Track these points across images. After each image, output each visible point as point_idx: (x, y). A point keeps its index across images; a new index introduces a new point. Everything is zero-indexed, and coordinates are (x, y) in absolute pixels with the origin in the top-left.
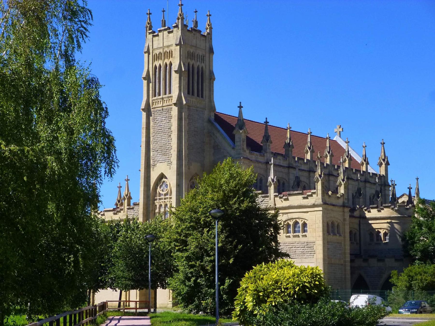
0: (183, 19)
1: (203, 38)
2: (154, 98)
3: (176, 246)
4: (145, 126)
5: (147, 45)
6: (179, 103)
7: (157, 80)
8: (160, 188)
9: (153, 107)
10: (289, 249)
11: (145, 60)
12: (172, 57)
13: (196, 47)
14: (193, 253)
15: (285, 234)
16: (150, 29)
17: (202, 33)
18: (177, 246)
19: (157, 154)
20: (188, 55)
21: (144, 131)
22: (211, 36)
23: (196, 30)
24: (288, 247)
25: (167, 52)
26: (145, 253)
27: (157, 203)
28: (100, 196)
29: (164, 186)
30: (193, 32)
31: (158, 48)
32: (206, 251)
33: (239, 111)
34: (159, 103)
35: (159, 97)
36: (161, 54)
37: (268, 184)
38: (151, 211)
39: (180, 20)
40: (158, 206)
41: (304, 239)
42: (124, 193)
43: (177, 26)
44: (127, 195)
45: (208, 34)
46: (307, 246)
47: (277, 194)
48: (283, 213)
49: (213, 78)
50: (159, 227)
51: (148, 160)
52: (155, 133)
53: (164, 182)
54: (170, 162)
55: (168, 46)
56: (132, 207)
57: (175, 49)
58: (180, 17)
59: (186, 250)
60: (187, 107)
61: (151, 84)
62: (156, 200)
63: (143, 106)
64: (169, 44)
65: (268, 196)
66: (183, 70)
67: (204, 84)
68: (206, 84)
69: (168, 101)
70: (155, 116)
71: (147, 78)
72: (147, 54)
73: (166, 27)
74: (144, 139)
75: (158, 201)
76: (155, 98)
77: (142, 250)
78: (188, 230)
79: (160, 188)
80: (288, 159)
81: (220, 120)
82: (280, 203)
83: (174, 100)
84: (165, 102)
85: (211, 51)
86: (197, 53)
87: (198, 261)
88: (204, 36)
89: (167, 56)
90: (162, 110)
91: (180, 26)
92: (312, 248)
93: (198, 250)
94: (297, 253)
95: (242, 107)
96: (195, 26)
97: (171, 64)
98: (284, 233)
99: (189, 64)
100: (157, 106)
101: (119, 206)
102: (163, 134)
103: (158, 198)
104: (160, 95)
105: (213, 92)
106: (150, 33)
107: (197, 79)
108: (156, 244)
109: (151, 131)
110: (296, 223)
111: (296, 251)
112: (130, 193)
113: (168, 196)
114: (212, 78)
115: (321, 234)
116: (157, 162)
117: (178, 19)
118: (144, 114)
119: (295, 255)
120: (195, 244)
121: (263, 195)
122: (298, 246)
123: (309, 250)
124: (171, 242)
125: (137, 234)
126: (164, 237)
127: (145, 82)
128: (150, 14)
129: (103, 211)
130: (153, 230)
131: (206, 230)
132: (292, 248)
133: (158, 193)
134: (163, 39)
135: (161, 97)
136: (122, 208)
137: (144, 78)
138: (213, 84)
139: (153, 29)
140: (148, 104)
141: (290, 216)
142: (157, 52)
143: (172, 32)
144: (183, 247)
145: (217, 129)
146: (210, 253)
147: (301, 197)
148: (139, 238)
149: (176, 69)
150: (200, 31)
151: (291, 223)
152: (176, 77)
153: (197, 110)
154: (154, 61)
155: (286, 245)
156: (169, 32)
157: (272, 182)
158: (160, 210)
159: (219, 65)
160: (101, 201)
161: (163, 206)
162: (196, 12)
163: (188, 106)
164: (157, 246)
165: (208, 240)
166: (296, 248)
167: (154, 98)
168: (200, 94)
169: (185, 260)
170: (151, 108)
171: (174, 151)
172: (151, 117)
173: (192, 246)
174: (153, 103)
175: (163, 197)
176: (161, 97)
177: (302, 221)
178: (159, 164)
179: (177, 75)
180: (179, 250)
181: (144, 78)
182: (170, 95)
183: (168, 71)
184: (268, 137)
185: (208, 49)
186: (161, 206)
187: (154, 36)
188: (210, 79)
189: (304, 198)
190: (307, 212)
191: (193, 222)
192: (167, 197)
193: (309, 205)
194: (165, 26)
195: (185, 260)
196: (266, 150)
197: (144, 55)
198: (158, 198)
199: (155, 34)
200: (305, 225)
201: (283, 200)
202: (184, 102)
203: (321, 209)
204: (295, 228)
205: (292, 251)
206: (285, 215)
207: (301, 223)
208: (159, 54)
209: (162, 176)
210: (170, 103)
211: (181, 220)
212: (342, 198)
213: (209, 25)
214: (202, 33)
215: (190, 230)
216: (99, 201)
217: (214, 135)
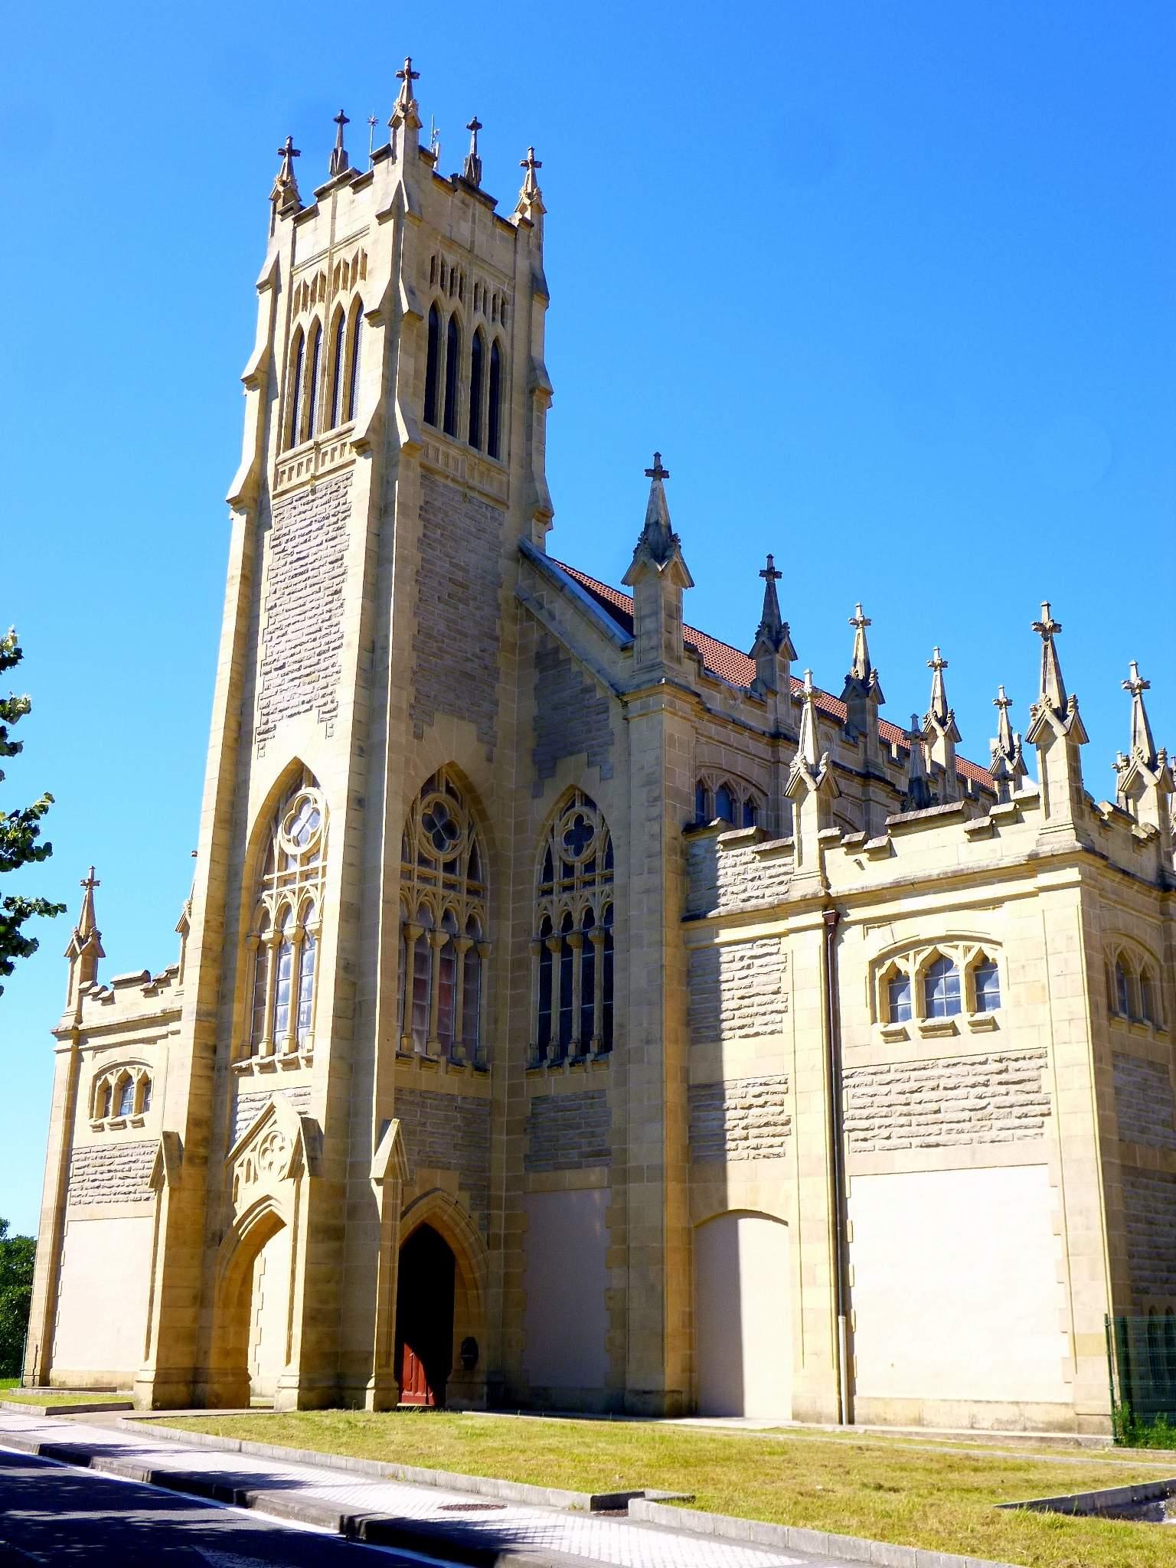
0: (414, 125)
1: (499, 230)
2: (283, 456)
4: (239, 572)
6: (377, 443)
7: (298, 389)
10: (902, 1099)
12: (364, 277)
15: (880, 1026)
17: (498, 210)
24: (899, 1087)
33: (653, 491)
37: (789, 787)
38: (241, 937)
40: (273, 915)
41: (986, 1043)
46: (1004, 1077)
47: (835, 831)
48: (868, 923)
51: (240, 725)
52: (278, 594)
53: (305, 800)
54: (330, 706)
55: (349, 241)
61: (276, 405)
62: (266, 886)
65: (791, 847)
67: (505, 408)
68: (512, 407)
71: (263, 380)
72: (268, 294)
75: (274, 891)
79: (288, 831)
80: (861, 745)
82: (848, 873)
84: (328, 458)
85: (538, 287)
89: (345, 281)
92: (1027, 1086)
94: (948, 1117)
98: (874, 1021)
99: (434, 309)
102: (309, 591)
103: (276, 874)
107: (469, 374)
109: (265, 588)
110: (937, 965)
111: (943, 1105)
114: (538, 389)
115: (1081, 1006)
117: (395, 124)
118: (239, 522)
119: (935, 1129)
121: (766, 846)
122: (951, 1083)
123: (1011, 1099)
132: (919, 1090)
134: (334, 217)
137: (250, 382)
138: (542, 422)
140: (257, 484)
141: (904, 931)
142: (307, 276)
147: (957, 832)
150: (490, 202)
151: (910, 966)
155: (888, 1077)
156: (357, 186)
157: (807, 778)
158: (280, 932)
161: (295, 911)
162: (476, 126)
166: (940, 1094)
168: (486, 436)
170: (271, 494)
172: (267, 534)
174: (278, 475)
177: (968, 949)
178: (286, 721)
184: (778, 633)
185: (522, 279)
186: (285, 910)
187: (298, 221)
189: (975, 834)
190: (996, 903)
193: (1006, 862)
196: (773, 682)
198: (276, 874)
200: (983, 970)
201: (863, 857)
203: (1073, 874)
204: (929, 993)
205: (919, 1108)
206: (874, 933)
207: (961, 959)
208: (315, 282)
209: (297, 777)
212: (1152, 846)
213: (529, 196)
214: (498, 210)
217: (541, 607)
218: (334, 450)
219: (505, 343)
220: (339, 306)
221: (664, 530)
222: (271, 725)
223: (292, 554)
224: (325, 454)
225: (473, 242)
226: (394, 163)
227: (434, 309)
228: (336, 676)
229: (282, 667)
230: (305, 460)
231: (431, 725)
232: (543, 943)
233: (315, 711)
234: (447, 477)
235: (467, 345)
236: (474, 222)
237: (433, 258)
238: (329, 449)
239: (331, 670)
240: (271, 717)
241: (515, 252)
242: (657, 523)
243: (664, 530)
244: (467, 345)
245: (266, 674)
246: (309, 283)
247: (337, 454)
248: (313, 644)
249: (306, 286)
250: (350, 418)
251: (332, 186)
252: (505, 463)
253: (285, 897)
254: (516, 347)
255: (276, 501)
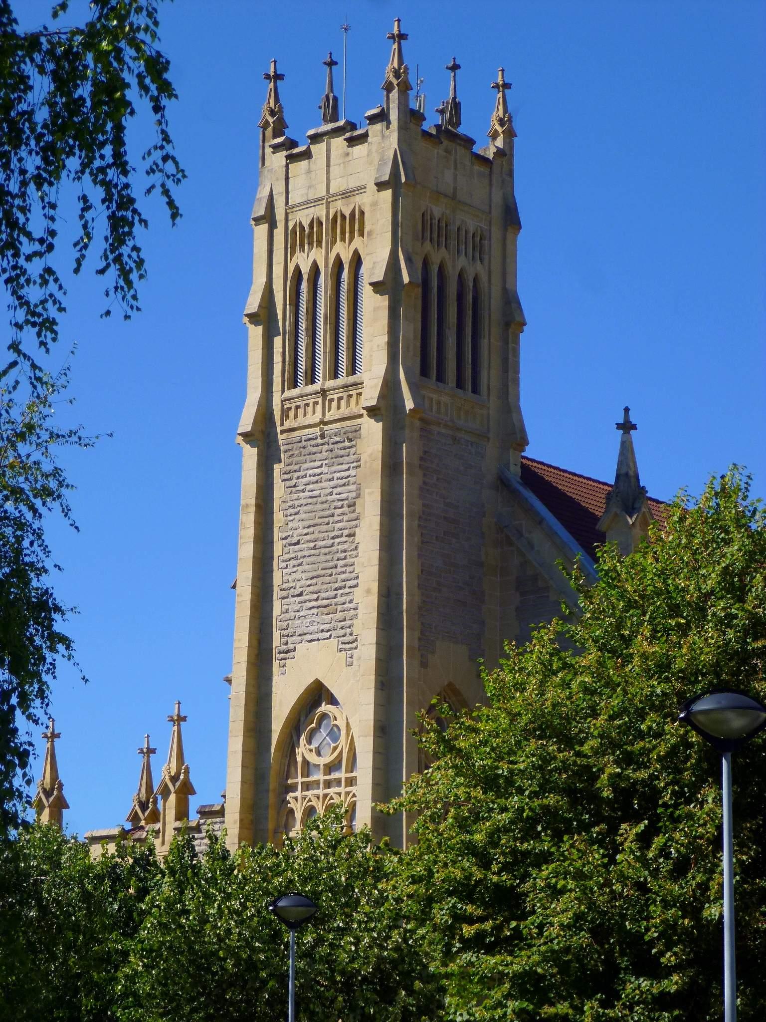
0: (405, 88)
1: (477, 168)
2: (288, 394)
3: (460, 918)
5: (264, 193)
6: (386, 408)
8: (309, 742)
9: (287, 425)
11: (256, 250)
12: (362, 234)
13: (454, 197)
14: (553, 957)
16: (276, 134)
17: (477, 149)
18: (471, 921)
19: (297, 607)
20: (424, 224)
21: (248, 521)
22: (511, 163)
23: (454, 137)
25: (343, 217)
26: (264, 982)
27: (296, 802)
28: (57, 609)
29: (323, 732)
30: (446, 143)
31: (307, 204)
32: (635, 944)
33: (623, 443)
34: (310, 409)
35: (311, 388)
36: (320, 224)
39: (394, 95)
40: (299, 815)
42: (164, 769)
43: (382, 117)
44: (174, 779)
45: (500, 153)
49: (518, 319)
50: (331, 868)
51: (260, 642)
53: (324, 716)
55: (346, 194)
56: (193, 824)
57: (374, 204)
58: (395, 82)
59: (514, 943)
60: (417, 423)
61: (278, 341)
62: (293, 788)
63: (246, 421)
64: (352, 185)
66: (406, 279)
67: (484, 342)
68: (490, 342)
69: (343, 403)
70: (295, 459)
71: (265, 316)
72: (264, 228)
73: (341, 123)
74: (246, 550)
75: (298, 794)
76: (295, 392)
77: (252, 966)
78: (530, 834)
79: (309, 742)
81: (542, 487)
83: (371, 395)
84: (334, 404)
85: (511, 218)
86: (458, 223)
87: (590, 998)
88: (484, 160)
89: (343, 233)
90: (323, 436)
91: (394, 116)
93: (583, 938)
95: (634, 427)
96: (450, 122)
97: (357, 261)
99: (426, 263)
100: (302, 421)
101: (143, 823)
103: (300, 780)
104: (313, 382)
105: (517, 372)
106: (276, 148)
107: (458, 320)
108: (319, 941)
109: (278, 517)
112: (187, 772)
113: (342, 775)
114: (512, 319)
116: (297, 639)
117: (389, 88)
118: (250, 455)
120: (563, 911)
124: (429, 901)
125: (228, 897)
126: (394, 874)
127: (256, 333)
128: (278, 77)
129: (43, 212)
130: (305, 881)
131: (629, 832)
133: (299, 760)
134: (328, 166)
135: (317, 387)
136: (158, 826)
137: (254, 318)
138: (517, 341)
139: (289, 133)
142: (304, 217)
143: (364, 138)
144: (498, 928)
145: (530, 510)
146: (662, 954)
148: (238, 913)
149: (379, 276)
150: (469, 142)
152: (376, 309)
153: (454, 439)
154: (294, 252)
156: (352, 141)
159: (541, 275)
160: (66, 641)
162: (455, 67)
163: (422, 420)
164: (323, 950)
165: (642, 887)
167: (288, 394)
168: (469, 379)
169: (509, 996)
170: (279, 429)
171: (368, 591)
172: (277, 467)
173: (554, 919)
174: (284, 412)
175: (318, 776)
176: (317, 387)
178: (305, 645)
179: (383, 302)
180: (476, 943)
181: (254, 318)
182: (351, 379)
183: (344, 287)
185: (497, 213)
187: (291, 158)
188: (507, 325)
191: (555, 789)
192: (335, 775)
194: (335, 119)
195: (509, 996)
197: (253, 230)
198: (300, 780)
199: (296, 151)
202: (409, 404)
209: (317, 695)
210: (354, 409)
211: (490, 782)
213: (501, 122)
214: (477, 149)
215: (537, 836)
216: (56, 639)
217: (521, 535)
218: (340, 399)
219: (484, 278)
220: (338, 256)
221: (633, 480)
222: (291, 646)
223: (303, 491)
224: (331, 400)
225: (455, 189)
226: (388, 128)
227: (426, 263)
228: (352, 612)
229: (300, 595)
230: (311, 402)
231: (434, 653)
232: (45, 252)
233: (334, 641)
234: (439, 424)
235: (452, 290)
236: (456, 168)
237: (423, 215)
238: (335, 397)
239: (347, 605)
240: (291, 639)
241: (491, 185)
242: (627, 474)
243: (633, 480)
244: (452, 290)
245: (284, 598)
246: (306, 224)
247: (343, 403)
248: (328, 579)
249: (302, 228)
250: (354, 373)
251: (326, 133)
252: (485, 397)
253: (310, 800)
254: (493, 281)
255: (285, 436)
